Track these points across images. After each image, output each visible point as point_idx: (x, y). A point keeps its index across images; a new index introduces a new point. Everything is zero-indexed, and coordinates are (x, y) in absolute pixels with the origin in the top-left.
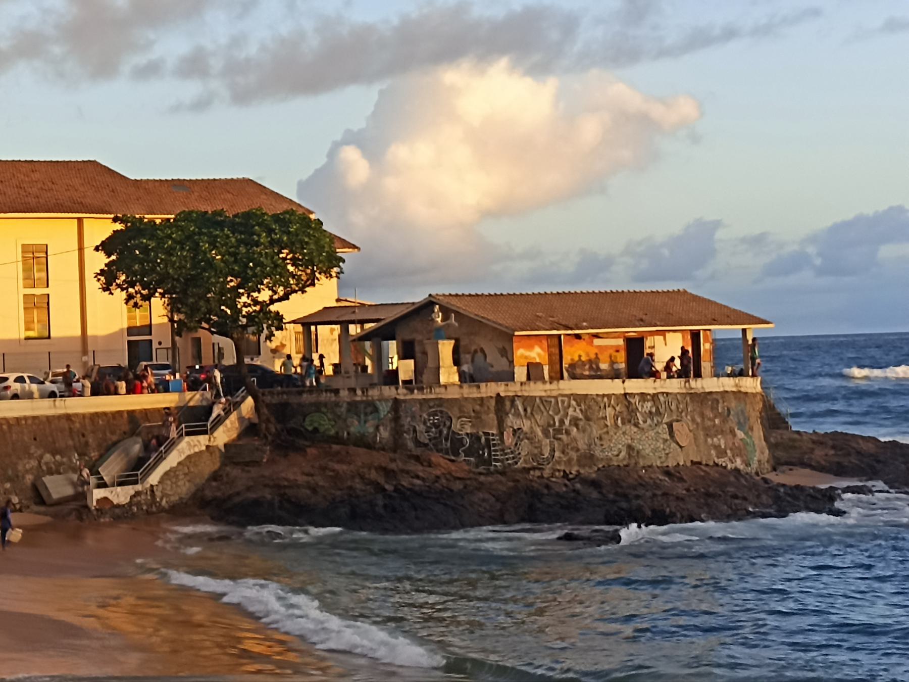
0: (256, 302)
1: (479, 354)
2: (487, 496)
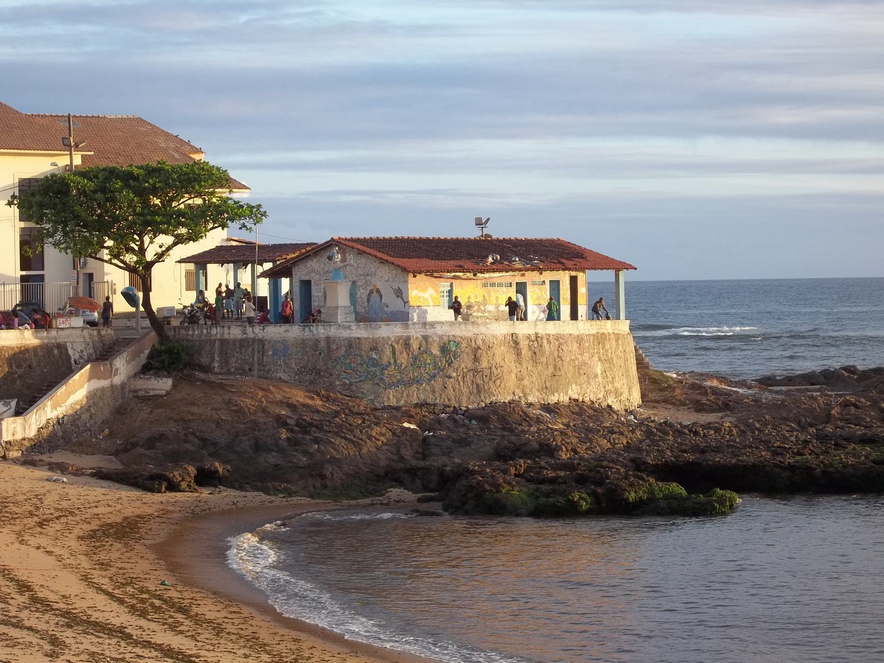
0: (91, 234)
1: (375, 294)
2: (384, 430)
